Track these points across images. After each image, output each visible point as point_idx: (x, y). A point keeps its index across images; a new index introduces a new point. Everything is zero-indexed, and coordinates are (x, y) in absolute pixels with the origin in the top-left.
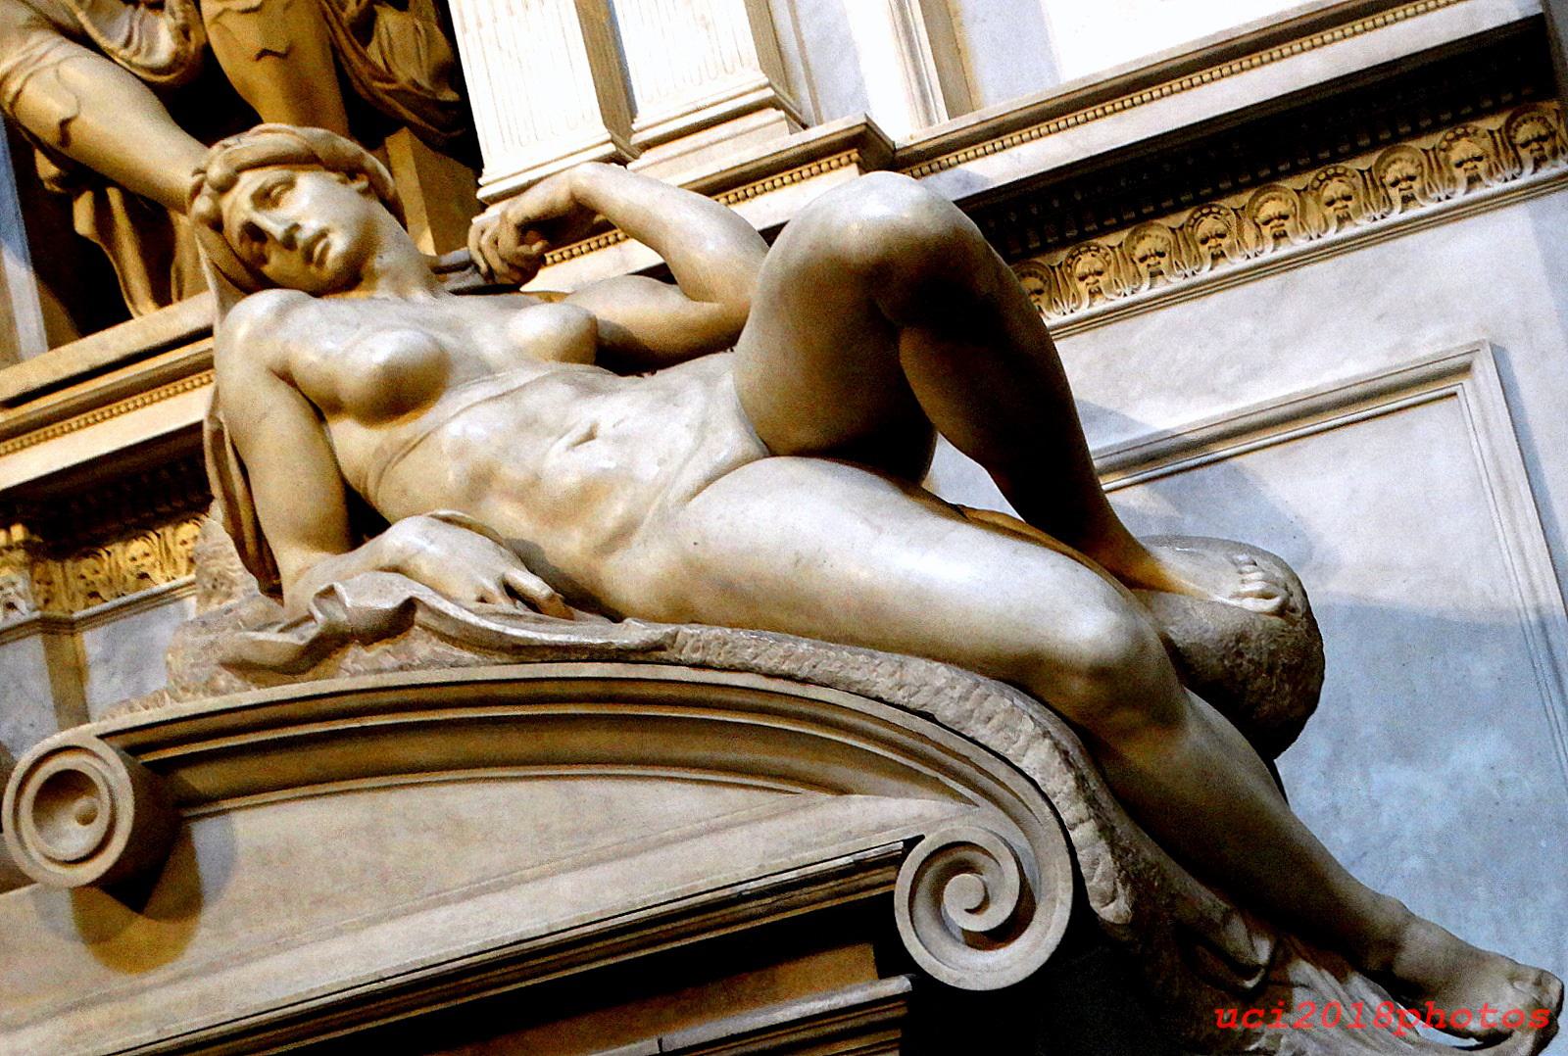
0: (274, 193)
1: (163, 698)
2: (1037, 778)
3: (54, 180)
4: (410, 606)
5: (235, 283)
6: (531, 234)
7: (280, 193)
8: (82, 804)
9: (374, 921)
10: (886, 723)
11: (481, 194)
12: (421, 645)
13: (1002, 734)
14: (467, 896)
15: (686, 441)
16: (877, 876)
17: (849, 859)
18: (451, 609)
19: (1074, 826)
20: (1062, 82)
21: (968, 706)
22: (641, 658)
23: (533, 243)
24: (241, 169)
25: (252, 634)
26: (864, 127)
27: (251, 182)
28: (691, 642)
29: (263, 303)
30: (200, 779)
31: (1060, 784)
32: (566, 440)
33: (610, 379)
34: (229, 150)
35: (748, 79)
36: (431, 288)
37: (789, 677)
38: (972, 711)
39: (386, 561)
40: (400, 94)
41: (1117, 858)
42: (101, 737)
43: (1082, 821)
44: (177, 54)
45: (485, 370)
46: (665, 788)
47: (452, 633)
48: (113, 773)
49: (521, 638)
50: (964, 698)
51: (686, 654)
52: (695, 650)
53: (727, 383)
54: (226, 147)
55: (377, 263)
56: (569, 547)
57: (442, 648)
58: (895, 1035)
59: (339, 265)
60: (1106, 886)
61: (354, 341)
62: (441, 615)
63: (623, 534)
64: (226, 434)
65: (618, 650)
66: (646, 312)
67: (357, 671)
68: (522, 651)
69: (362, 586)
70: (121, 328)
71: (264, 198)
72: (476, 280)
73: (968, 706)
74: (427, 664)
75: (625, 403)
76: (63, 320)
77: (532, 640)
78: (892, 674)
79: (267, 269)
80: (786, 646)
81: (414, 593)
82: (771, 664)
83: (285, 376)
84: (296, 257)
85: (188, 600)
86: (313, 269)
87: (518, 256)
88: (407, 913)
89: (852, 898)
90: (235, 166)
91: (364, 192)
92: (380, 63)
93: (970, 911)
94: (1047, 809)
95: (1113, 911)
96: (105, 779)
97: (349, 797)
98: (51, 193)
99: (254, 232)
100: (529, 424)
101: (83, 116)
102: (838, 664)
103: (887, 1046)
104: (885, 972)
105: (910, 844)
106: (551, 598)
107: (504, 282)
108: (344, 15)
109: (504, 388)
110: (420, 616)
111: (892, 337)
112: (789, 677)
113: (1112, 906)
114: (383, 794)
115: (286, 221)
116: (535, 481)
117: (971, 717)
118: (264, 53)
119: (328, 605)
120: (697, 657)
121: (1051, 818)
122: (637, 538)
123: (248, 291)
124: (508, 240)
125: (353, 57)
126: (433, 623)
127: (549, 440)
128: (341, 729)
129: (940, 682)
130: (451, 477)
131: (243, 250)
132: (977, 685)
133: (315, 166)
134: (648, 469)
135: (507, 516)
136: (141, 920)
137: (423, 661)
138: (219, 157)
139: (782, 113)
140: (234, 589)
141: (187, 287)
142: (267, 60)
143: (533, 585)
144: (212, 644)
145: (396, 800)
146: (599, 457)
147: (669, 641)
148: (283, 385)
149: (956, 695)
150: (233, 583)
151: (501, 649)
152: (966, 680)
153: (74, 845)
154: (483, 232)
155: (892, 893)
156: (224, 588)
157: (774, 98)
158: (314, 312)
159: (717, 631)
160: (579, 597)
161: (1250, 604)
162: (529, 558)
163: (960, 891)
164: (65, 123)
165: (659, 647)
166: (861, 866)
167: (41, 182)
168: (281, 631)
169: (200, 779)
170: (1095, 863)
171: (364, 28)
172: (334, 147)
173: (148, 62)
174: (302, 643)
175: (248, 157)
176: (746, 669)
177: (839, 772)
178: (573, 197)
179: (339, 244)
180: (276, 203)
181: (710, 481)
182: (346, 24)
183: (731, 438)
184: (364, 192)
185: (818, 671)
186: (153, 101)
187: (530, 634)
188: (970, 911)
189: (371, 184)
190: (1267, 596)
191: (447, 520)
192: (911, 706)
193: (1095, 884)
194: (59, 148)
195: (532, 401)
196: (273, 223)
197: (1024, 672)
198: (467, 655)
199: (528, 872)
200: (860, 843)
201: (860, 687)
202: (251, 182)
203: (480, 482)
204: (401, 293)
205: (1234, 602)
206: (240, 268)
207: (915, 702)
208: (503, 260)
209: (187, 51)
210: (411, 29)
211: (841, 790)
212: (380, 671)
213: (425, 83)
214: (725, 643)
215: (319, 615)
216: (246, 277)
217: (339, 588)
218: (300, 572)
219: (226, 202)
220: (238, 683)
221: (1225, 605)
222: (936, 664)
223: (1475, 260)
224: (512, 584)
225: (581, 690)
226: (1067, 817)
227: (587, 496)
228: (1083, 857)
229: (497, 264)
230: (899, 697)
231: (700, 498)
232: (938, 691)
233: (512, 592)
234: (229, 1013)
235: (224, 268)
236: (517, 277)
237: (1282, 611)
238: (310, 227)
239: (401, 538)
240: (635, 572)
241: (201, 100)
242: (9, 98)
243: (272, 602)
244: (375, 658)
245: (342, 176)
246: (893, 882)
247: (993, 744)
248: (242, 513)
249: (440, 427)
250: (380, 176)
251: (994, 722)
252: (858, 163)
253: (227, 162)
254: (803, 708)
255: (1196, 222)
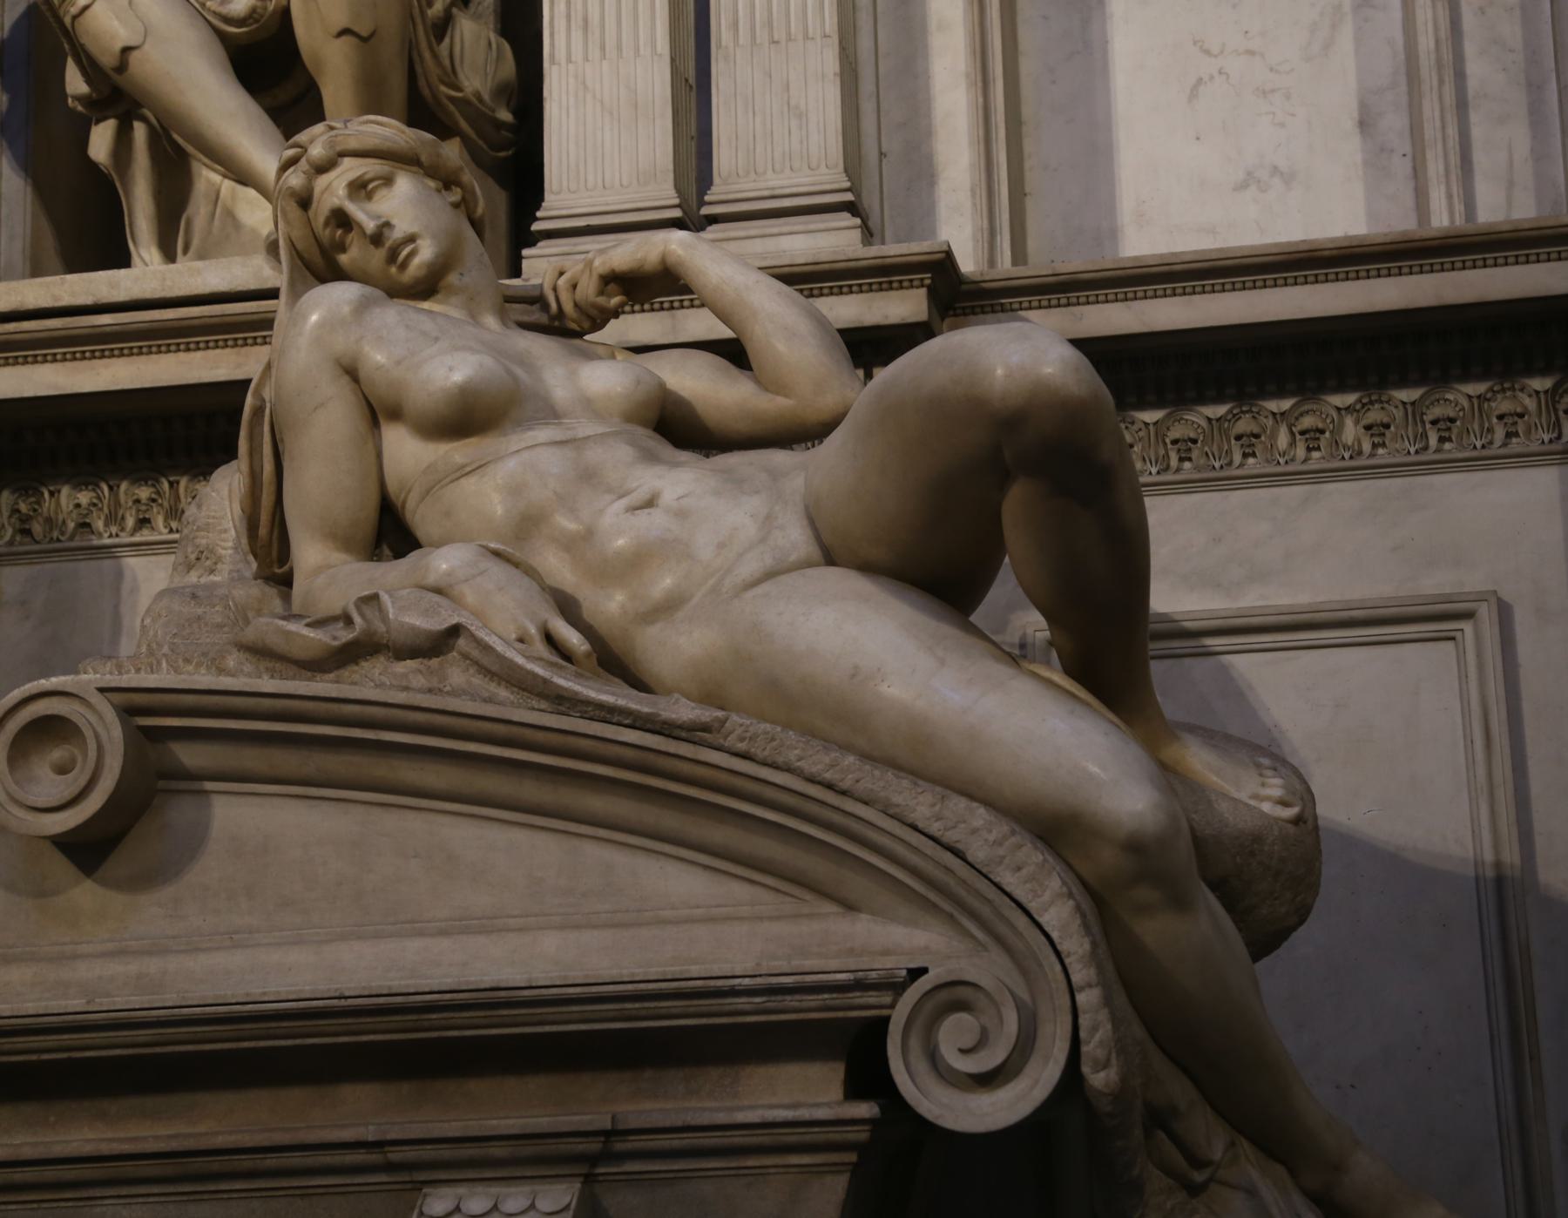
0: (370, 186)
1: (159, 663)
2: (1055, 935)
3: (77, 98)
4: (455, 631)
5: (308, 265)
6: (612, 287)
7: (376, 188)
8: (58, 754)
9: (343, 937)
10: (916, 850)
11: (536, 227)
12: (457, 675)
13: (1028, 886)
14: (443, 933)
15: (750, 529)
16: (871, 998)
17: (850, 976)
18: (492, 640)
19: (1082, 989)
20: (1122, 255)
21: (1001, 851)
22: (684, 734)
23: (610, 296)
24: (342, 154)
25: (281, 623)
26: (942, 256)
27: (350, 169)
28: (739, 731)
29: (342, 294)
30: (189, 755)
31: (1076, 946)
32: (622, 504)
33: (667, 450)
34: (333, 133)
35: (828, 176)
36: (503, 317)
37: (830, 786)
38: (1003, 857)
39: (431, 579)
40: (463, 104)
41: (1116, 1027)
42: (102, 690)
43: (1090, 986)
44: (254, 10)
45: (550, 413)
46: (672, 868)
47: (494, 668)
48: (107, 732)
49: (566, 689)
50: (998, 843)
51: (730, 742)
52: (742, 739)
53: (796, 484)
54: (332, 128)
55: (453, 278)
56: (609, 605)
57: (477, 680)
58: (852, 1157)
59: (423, 272)
60: (1101, 1054)
61: (440, 354)
62: (486, 648)
63: (668, 607)
64: (267, 411)
65: (665, 723)
66: (701, 384)
67: (375, 682)
68: (563, 701)
69: (400, 595)
70: (123, 272)
71: (360, 188)
72: (537, 316)
73: (1001, 851)
74: (454, 693)
75: (682, 481)
76: (49, 242)
77: (576, 693)
78: (933, 805)
79: (343, 259)
80: (833, 755)
81: (462, 620)
82: (814, 770)
83: (351, 371)
84: (379, 255)
85: (134, 564)
86: (393, 270)
87: (594, 306)
88: (378, 936)
89: (840, 1014)
90: (339, 148)
91: (456, 206)
92: (447, 62)
93: (961, 1051)
94: (1058, 967)
95: (1099, 1079)
96: (97, 736)
97: (342, 805)
98: (73, 111)
99: (341, 219)
100: (588, 477)
101: (146, 47)
102: (882, 784)
103: (834, 1169)
104: (854, 1091)
105: (916, 973)
106: (588, 655)
107: (566, 325)
108: (430, 12)
109: (569, 435)
110: (462, 642)
111: (1004, 478)
112: (830, 786)
113: (1102, 1074)
114: (377, 811)
115: (379, 217)
116: (589, 534)
117: (1000, 863)
118: (345, 32)
119: (368, 611)
120: (742, 746)
121: (1061, 976)
122: (680, 615)
123: (323, 280)
124: (588, 288)
125: (427, 55)
126: (475, 653)
127: (608, 497)
128: (345, 732)
129: (978, 823)
130: (499, 510)
131: (325, 235)
132: (1013, 833)
133: (415, 169)
134: (704, 546)
135: (558, 568)
136: (88, 884)
137: (456, 687)
138: (325, 137)
139: (858, 221)
140: (219, 566)
141: (195, 242)
142: (346, 39)
143: (573, 638)
144: (199, 618)
145: (391, 821)
146: (653, 523)
147: (716, 725)
148: (346, 379)
149: (991, 838)
150: (219, 559)
151: (541, 695)
152: (1002, 827)
153: (55, 796)
154: (561, 274)
155: (887, 1019)
156: (208, 563)
157: (851, 203)
158: (391, 315)
159: (768, 726)
160: (612, 661)
161: (1266, 807)
162: (567, 607)
163: (953, 1033)
164: (126, 50)
165: (706, 728)
166: (860, 985)
167: (65, 96)
168: (308, 625)
169: (189, 755)
170: (1095, 1029)
171: (441, 28)
172: (439, 155)
173: (224, 10)
174: (336, 643)
175: (353, 144)
176: (788, 769)
177: (856, 884)
178: (663, 261)
179: (426, 252)
180: (369, 196)
181: (769, 575)
182: (429, 23)
183: (795, 537)
184: (456, 206)
185: (861, 786)
186: (220, 53)
187: (577, 688)
188: (961, 1051)
189: (463, 199)
190: (1284, 803)
191: (497, 554)
192: (944, 840)
193: (1091, 1048)
194: (112, 74)
195: (594, 454)
196: (365, 216)
197: (1055, 829)
198: (503, 693)
199: (511, 921)
200: (864, 963)
201: (897, 810)
202: (350, 169)
203: (528, 524)
204: (474, 316)
205: (1252, 802)
206: (315, 250)
207: (950, 837)
208: (576, 305)
209: (265, 8)
210: (483, 43)
211: (850, 907)
212: (406, 689)
213: (486, 97)
214: (773, 739)
215: (357, 619)
216: (317, 259)
217: (385, 597)
218: (319, 570)
219: (322, 182)
220: (248, 668)
221: (1246, 805)
222: (975, 805)
223: (1482, 515)
224: (553, 633)
225: (601, 743)
226: (1076, 978)
227: (636, 562)
228: (1084, 1021)
229: (568, 307)
230: (935, 828)
231: (759, 590)
232: (974, 831)
233: (550, 639)
234: (171, 998)
235: (299, 246)
236: (586, 325)
237: (1298, 821)
238: (402, 228)
239: (443, 562)
240: (675, 648)
241: (267, 64)
242: (74, 10)
243: (272, 592)
244: (405, 675)
245: (440, 184)
246: (892, 1006)
247: (1019, 893)
248: (264, 496)
249: (499, 459)
250: (473, 193)
251: (1024, 872)
252: (929, 288)
253: (331, 144)
254: (837, 818)
255: (1236, 417)
